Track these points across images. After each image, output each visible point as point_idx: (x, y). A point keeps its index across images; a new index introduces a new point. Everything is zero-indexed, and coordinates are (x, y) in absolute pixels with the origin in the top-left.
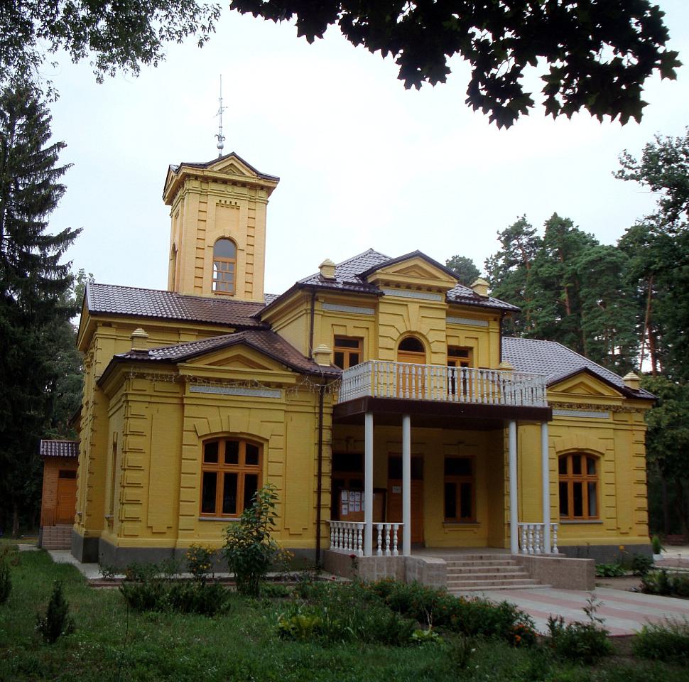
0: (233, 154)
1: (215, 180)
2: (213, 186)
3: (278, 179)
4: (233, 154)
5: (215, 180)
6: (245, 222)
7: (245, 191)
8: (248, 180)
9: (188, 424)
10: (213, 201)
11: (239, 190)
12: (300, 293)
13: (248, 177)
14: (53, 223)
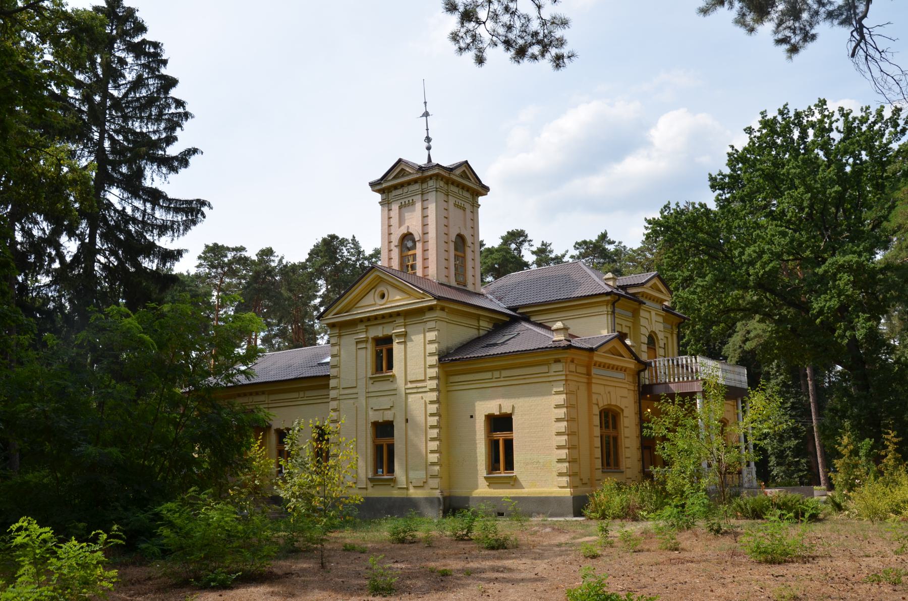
0: (466, 162)
1: (454, 183)
2: (453, 188)
4: (466, 162)
5: (454, 183)
8: (411, 177)
10: (452, 201)
12: (609, 298)
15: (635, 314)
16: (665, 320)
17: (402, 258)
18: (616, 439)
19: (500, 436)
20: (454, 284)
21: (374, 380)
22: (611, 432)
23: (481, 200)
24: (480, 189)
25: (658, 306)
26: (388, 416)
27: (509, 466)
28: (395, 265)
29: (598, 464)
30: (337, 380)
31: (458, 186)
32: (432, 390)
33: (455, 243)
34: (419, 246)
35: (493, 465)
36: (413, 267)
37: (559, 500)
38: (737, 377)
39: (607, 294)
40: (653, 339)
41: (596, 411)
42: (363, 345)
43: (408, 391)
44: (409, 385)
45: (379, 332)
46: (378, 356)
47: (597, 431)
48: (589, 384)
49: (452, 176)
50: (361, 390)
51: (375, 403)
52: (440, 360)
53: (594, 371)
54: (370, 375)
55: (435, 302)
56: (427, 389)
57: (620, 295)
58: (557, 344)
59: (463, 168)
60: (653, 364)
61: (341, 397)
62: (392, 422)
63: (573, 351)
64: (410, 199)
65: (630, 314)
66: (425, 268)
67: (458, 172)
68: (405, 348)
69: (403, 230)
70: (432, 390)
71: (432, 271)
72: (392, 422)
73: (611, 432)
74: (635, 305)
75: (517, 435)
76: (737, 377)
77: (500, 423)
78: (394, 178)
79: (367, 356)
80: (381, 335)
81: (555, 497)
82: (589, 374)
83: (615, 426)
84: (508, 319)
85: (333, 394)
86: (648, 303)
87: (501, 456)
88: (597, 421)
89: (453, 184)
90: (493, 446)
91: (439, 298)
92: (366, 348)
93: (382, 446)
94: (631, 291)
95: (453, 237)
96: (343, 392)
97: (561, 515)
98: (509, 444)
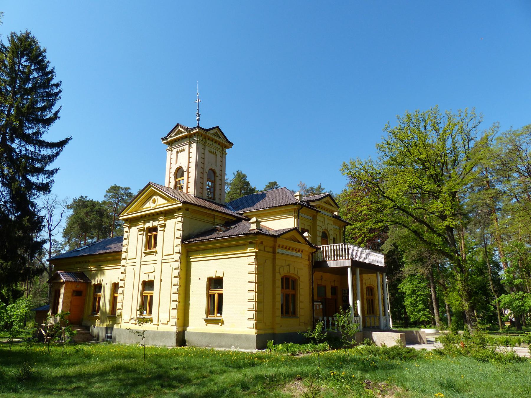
0: (218, 127)
2: (208, 141)
3: (233, 144)
4: (218, 127)
6: (219, 163)
7: (219, 147)
8: (220, 141)
9: (277, 270)
11: (217, 145)
12: (295, 207)
13: (222, 140)
14: (51, 134)
15: (314, 218)
16: (334, 223)
17: (176, 183)
18: (294, 296)
19: (216, 292)
20: (206, 198)
21: (146, 254)
22: (290, 292)
23: (228, 151)
24: (227, 144)
25: (330, 214)
26: (151, 278)
27: (220, 311)
28: (172, 186)
29: (279, 312)
30: (126, 254)
31: (212, 141)
32: (176, 261)
33: (208, 174)
34: (186, 174)
35: (210, 311)
36: (182, 188)
37: (247, 337)
38: (378, 259)
39: (295, 204)
40: (326, 235)
41: (278, 277)
42: (142, 232)
43: (142, 263)
44: (165, 257)
45: (150, 224)
46: (149, 239)
47: (278, 290)
48: (274, 259)
49: (207, 134)
50: (138, 260)
51: (144, 269)
52: (182, 241)
53: (278, 250)
54: (143, 251)
55: (181, 205)
56: (174, 260)
57: (303, 205)
58: (251, 232)
59: (216, 130)
60: (322, 249)
61: (127, 265)
62: (153, 281)
63: (261, 236)
64: (183, 147)
65: (311, 218)
66: (188, 188)
67: (212, 132)
68: (271, 252)
69: (178, 166)
70: (176, 261)
71: (191, 191)
72: (153, 281)
73: (290, 292)
74: (314, 213)
75: (227, 291)
76: (378, 259)
77: (216, 283)
78: (175, 135)
79: (142, 239)
80: (151, 226)
81: (245, 335)
82: (274, 252)
83: (294, 287)
84: (235, 219)
85: (123, 262)
86: (322, 211)
87: (215, 305)
88: (279, 283)
89: (209, 139)
90: (210, 298)
91: (184, 202)
92: (143, 235)
93: (214, 295)
94: (312, 204)
95: (207, 170)
96: (128, 261)
97: (249, 348)
98: (220, 296)
